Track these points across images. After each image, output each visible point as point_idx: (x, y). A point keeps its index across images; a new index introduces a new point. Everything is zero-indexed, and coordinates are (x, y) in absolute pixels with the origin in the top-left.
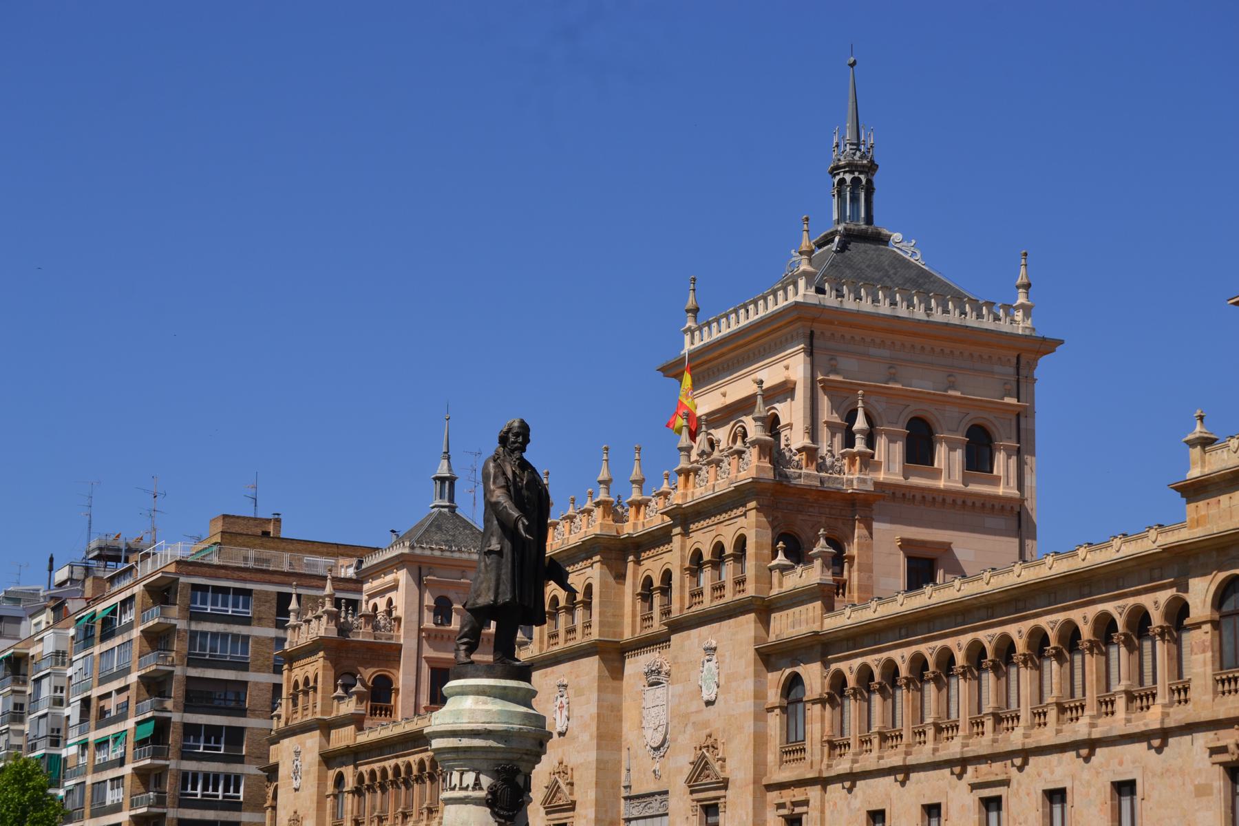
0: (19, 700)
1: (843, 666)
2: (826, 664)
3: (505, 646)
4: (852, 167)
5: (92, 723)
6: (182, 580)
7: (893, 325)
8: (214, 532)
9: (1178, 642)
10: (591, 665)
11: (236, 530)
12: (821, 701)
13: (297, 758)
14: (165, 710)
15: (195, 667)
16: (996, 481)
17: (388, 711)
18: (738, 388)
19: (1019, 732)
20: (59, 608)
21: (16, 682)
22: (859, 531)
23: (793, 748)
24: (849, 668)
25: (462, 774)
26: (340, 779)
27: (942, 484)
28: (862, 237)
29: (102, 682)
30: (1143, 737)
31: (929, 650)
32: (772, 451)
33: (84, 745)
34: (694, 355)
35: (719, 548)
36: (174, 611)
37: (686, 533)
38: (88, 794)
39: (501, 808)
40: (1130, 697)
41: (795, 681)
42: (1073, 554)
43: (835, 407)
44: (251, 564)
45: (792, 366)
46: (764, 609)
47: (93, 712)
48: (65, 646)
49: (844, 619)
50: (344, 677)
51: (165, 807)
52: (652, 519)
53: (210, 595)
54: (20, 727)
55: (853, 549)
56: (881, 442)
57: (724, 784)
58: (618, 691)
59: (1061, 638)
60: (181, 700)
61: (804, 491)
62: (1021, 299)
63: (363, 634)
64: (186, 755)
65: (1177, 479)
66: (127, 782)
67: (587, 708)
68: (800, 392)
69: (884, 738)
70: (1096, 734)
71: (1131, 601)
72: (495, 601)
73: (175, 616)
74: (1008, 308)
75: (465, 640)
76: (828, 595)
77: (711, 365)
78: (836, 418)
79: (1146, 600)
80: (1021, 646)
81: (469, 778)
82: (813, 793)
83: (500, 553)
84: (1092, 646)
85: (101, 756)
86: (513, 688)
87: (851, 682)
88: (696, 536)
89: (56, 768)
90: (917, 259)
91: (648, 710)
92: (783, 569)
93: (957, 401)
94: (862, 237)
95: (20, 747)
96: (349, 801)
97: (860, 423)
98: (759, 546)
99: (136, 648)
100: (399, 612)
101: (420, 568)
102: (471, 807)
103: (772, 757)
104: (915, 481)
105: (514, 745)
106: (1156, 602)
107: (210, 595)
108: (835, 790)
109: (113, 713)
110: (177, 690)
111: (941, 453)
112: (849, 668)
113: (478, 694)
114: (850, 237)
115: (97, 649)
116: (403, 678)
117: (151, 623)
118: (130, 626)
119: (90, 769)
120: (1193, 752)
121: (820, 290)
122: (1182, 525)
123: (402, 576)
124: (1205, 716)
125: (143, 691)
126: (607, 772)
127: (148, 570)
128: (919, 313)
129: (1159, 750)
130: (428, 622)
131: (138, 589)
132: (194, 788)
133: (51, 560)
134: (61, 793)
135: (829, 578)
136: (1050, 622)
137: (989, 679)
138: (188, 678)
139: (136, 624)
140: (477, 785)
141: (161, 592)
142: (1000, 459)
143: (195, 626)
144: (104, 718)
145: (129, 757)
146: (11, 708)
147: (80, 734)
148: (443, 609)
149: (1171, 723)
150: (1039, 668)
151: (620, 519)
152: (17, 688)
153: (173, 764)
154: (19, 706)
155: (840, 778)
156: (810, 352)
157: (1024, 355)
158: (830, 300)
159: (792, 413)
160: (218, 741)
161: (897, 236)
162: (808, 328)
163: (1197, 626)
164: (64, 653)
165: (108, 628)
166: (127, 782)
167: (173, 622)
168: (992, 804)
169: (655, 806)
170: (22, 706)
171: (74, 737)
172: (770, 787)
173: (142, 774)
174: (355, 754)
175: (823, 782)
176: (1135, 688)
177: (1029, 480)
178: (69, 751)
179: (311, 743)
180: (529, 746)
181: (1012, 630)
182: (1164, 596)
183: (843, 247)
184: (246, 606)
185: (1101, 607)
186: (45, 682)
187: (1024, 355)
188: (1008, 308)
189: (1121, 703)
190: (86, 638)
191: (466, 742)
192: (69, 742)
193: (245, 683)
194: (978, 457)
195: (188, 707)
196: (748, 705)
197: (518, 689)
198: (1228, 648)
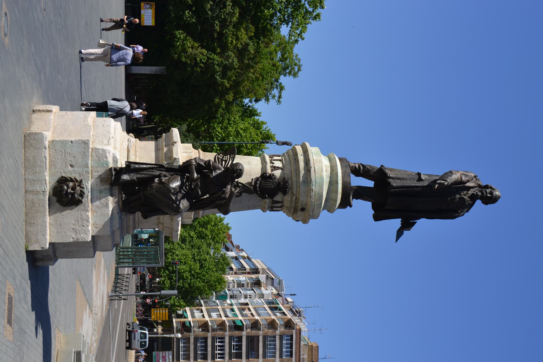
0: (245, 285)
3: (361, 193)
5: (240, 307)
6: (294, 331)
8: (312, 343)
14: (246, 329)
15: (263, 338)
21: (252, 284)
25: (280, 160)
29: (255, 308)
33: (232, 305)
36: (283, 329)
38: (214, 307)
39: (261, 183)
44: (302, 357)
48: (266, 297)
51: (212, 332)
53: (289, 342)
54: (236, 287)
60: (250, 335)
64: (231, 338)
66: (220, 319)
72: (390, 177)
73: (280, 330)
75: (362, 168)
81: (278, 164)
83: (420, 179)
86: (337, 188)
89: (223, 298)
95: (229, 287)
99: (269, 317)
102: (260, 166)
105: (302, 188)
107: (289, 342)
109: (244, 313)
110: (254, 333)
115: (266, 306)
117: (277, 321)
118: (275, 315)
119: (223, 307)
125: (253, 321)
127: (296, 320)
132: (219, 342)
133: (294, 295)
134: (214, 300)
138: (259, 336)
139: (276, 317)
140: (274, 168)
141: (289, 324)
143: (277, 337)
144: (241, 310)
145: (228, 318)
146: (242, 283)
147: (236, 304)
152: (249, 284)
153: (227, 333)
154: (243, 286)
160: (236, 349)
164: (263, 297)
165: (274, 309)
166: (220, 319)
167: (279, 329)
170: (243, 286)
171: (234, 301)
173: (223, 324)
178: (228, 301)
180: (301, 199)
184: (286, 356)
186: (253, 292)
190: (269, 303)
191: (301, 158)
192: (232, 300)
193: (258, 358)
195: (248, 337)
197: (337, 192)
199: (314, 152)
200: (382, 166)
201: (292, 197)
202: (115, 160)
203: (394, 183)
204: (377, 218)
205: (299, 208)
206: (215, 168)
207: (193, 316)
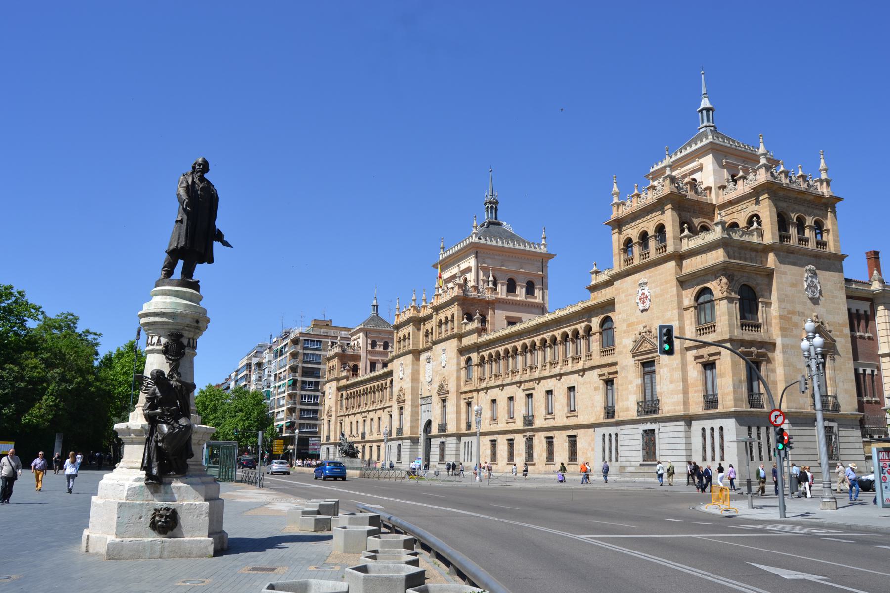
1: (483, 353)
2: (478, 353)
3: (188, 272)
4: (491, 202)
7: (503, 249)
9: (588, 340)
10: (410, 357)
11: (318, 324)
12: (477, 365)
13: (330, 389)
16: (536, 298)
17: (357, 375)
19: (538, 372)
20: (270, 348)
22: (491, 312)
23: (469, 380)
24: (486, 354)
26: (342, 396)
27: (518, 299)
28: (494, 224)
30: (577, 372)
31: (509, 347)
32: (463, 286)
34: (441, 262)
35: (447, 318)
37: (437, 314)
40: (573, 359)
41: (469, 359)
43: (484, 275)
45: (471, 262)
46: (460, 336)
49: (485, 338)
50: (343, 364)
52: (429, 311)
55: (488, 318)
56: (499, 286)
57: (448, 393)
58: (418, 365)
59: (551, 341)
61: (473, 299)
62: (543, 242)
63: (349, 352)
64: (302, 390)
65: (588, 285)
67: (409, 370)
68: (473, 270)
69: (496, 376)
70: (562, 372)
71: (573, 327)
73: (299, 349)
74: (539, 245)
76: (480, 331)
77: (446, 264)
78: (485, 278)
79: (578, 326)
80: (538, 344)
82: (475, 394)
84: (561, 343)
85: (280, 391)
87: (486, 358)
88: (440, 315)
89: (269, 394)
90: (511, 230)
91: (427, 370)
92: (466, 324)
93: (523, 274)
94: (494, 224)
96: (344, 402)
97: (491, 278)
98: (458, 317)
100: (361, 345)
101: (367, 332)
102: (156, 355)
103: (462, 384)
104: (510, 298)
105: (178, 321)
106: (581, 327)
108: (482, 393)
111: (518, 289)
112: (486, 354)
113: (163, 294)
114: (490, 224)
115: (279, 359)
116: (362, 365)
120: (593, 375)
121: (479, 238)
122: (589, 300)
123: (361, 334)
124: (597, 364)
126: (415, 390)
127: (292, 336)
128: (511, 246)
129: (582, 376)
130: (369, 348)
135: (479, 326)
136: (547, 336)
137: (528, 355)
139: (288, 351)
140: (159, 343)
141: (295, 342)
142: (537, 291)
144: (280, 379)
148: (374, 345)
149: (586, 367)
150: (544, 351)
151: (419, 311)
154: (260, 377)
155: (483, 389)
156: (476, 257)
157: (544, 259)
158: (483, 241)
159: (471, 276)
161: (505, 224)
162: (476, 250)
163: (595, 334)
165: (281, 353)
168: (529, 396)
169: (429, 400)
172: (462, 393)
173: (290, 396)
174: (346, 388)
175: (478, 391)
176: (575, 356)
177: (546, 298)
178: (272, 390)
179: (334, 385)
181: (535, 339)
182: (584, 325)
183: (488, 227)
185: (563, 330)
187: (544, 259)
188: (539, 245)
189: (570, 361)
190: (276, 357)
191: (152, 319)
194: (530, 289)
195: (302, 376)
196: (455, 367)
197: (185, 292)
198: (605, 341)
199: (147, 308)
202: (139, 480)
204: (211, 261)
206: (154, 393)
207: (282, 419)
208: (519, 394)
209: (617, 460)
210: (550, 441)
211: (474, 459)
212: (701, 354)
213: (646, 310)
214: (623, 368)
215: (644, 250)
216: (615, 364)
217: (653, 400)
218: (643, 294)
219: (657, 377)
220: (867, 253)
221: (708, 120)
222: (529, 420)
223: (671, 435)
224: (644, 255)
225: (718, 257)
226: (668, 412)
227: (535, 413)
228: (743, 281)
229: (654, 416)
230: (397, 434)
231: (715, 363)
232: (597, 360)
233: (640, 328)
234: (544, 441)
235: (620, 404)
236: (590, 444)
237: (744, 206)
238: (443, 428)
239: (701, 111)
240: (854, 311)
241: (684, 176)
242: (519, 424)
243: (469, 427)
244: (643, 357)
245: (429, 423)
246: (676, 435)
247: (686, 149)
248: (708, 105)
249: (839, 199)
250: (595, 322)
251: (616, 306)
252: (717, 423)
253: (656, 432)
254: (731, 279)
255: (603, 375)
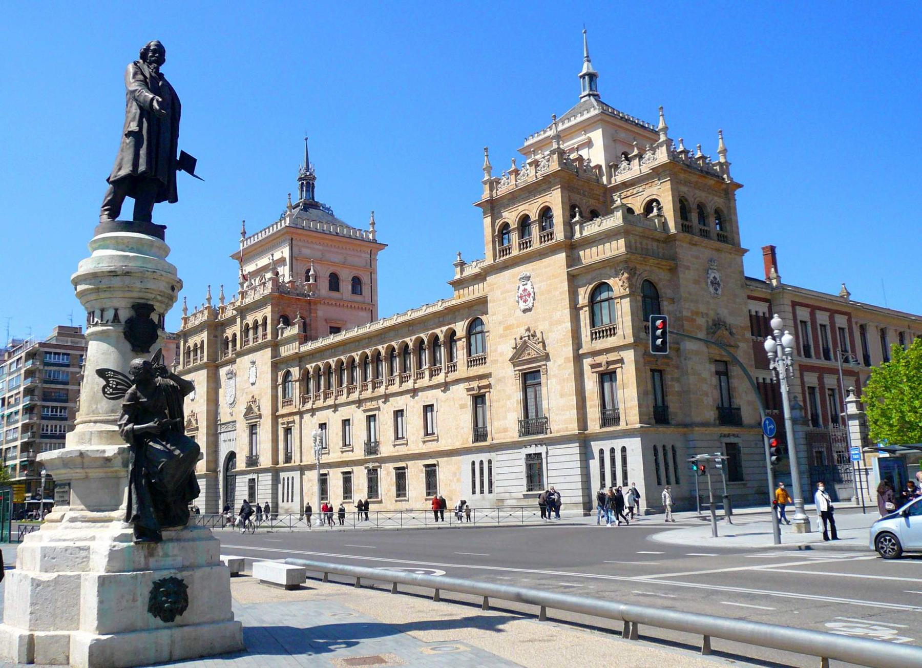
18: (263, 261)
29: (10, 391)
42: (406, 314)
47: (6, 403)
49: (309, 346)
52: (230, 313)
65: (451, 280)
82: (297, 418)
106: (441, 332)
112: (310, 367)
124: (464, 375)
131: (23, 354)
155: (307, 411)
163: (460, 339)
169: (230, 427)
200: (108, 180)
201: (158, 301)
202: (122, 538)
203: (142, 168)
204: (174, 199)
205: (170, 292)
207: (14, 458)
208: (358, 417)
209: (490, 492)
210: (401, 475)
211: (297, 498)
212: (597, 362)
213: (530, 310)
214: (499, 380)
215: (515, 241)
216: (488, 376)
217: (376, 442)
218: (525, 290)
219: (544, 390)
220: (763, 249)
221: (591, 89)
222: (371, 448)
223: (563, 459)
224: (524, 245)
225: (618, 247)
226: (558, 431)
227: (381, 439)
228: (645, 276)
229: (541, 436)
230: (319, 454)
231: (615, 372)
232: (462, 370)
233: (522, 331)
234: (393, 473)
235: (496, 424)
236: (455, 474)
237: (641, 189)
238: (252, 461)
239: (583, 77)
240: (754, 313)
241: (572, 150)
242: (359, 453)
243: (288, 459)
244: (525, 367)
245: (232, 456)
246: (568, 458)
247: (569, 119)
248: (591, 71)
249: (741, 186)
250: (460, 328)
251: (490, 305)
252: (618, 444)
253: (544, 456)
254: (632, 272)
255: (473, 389)
